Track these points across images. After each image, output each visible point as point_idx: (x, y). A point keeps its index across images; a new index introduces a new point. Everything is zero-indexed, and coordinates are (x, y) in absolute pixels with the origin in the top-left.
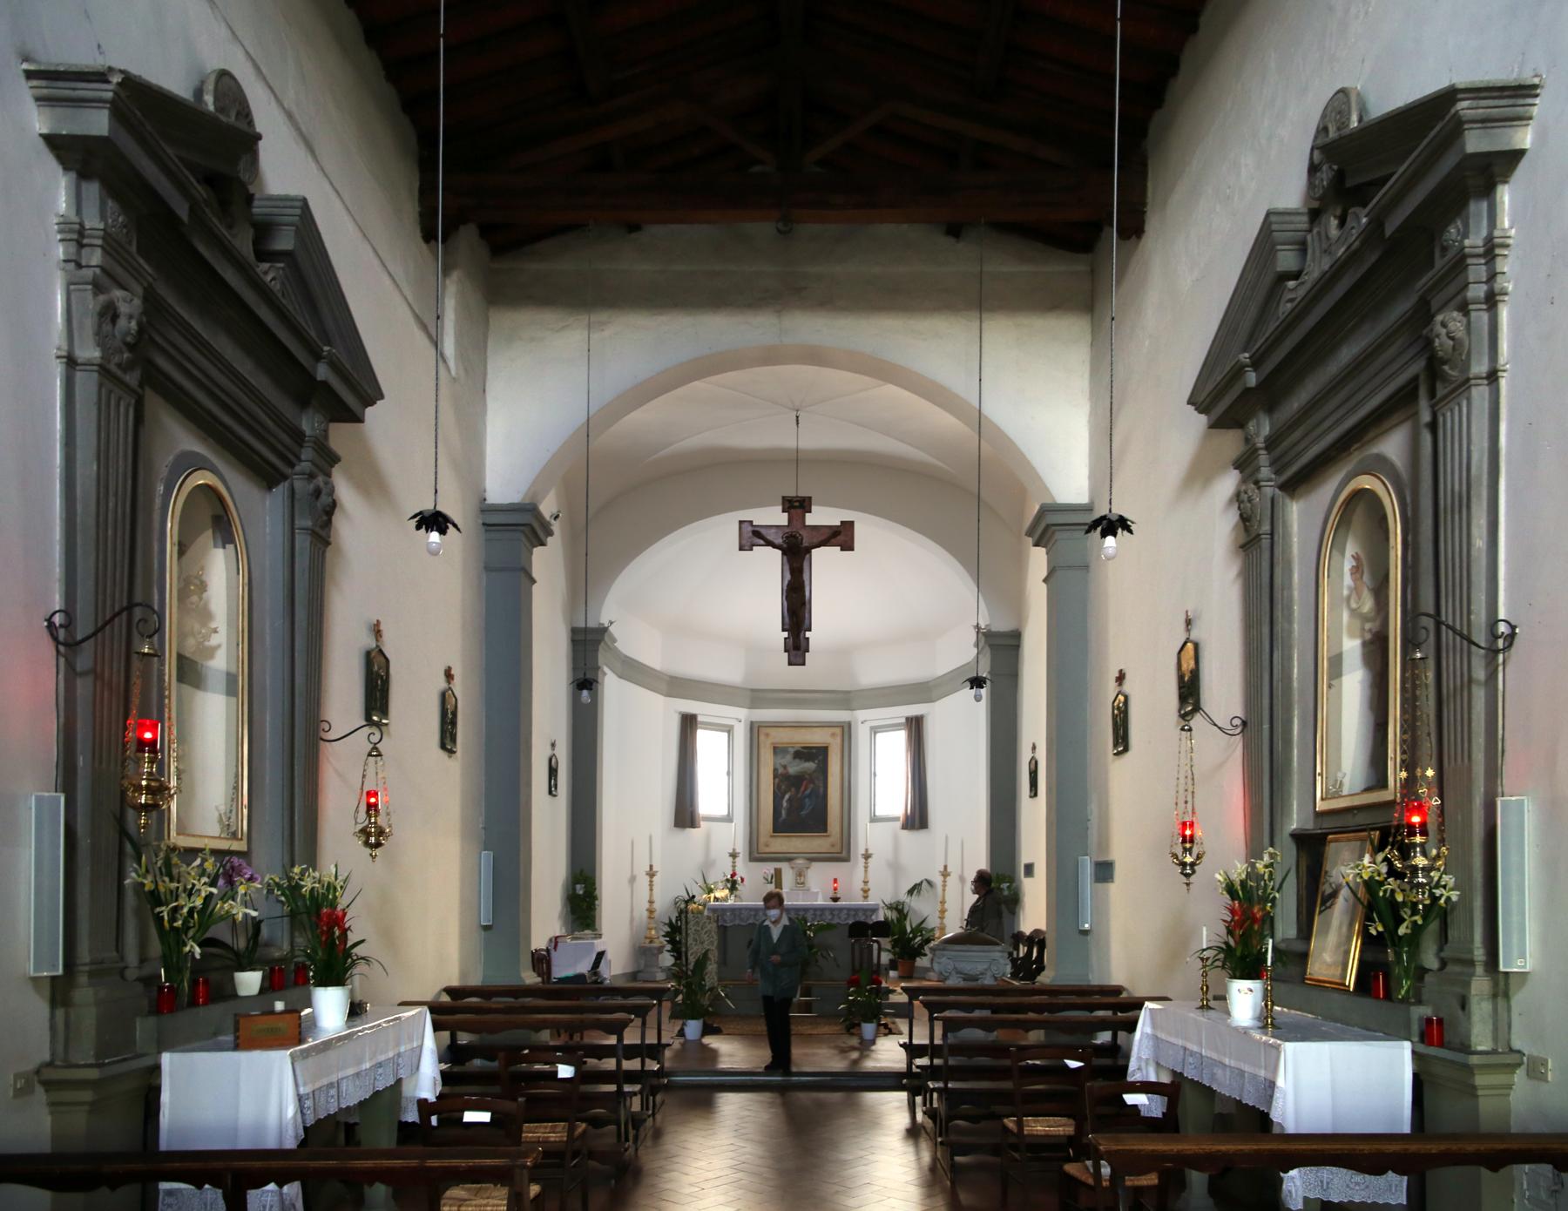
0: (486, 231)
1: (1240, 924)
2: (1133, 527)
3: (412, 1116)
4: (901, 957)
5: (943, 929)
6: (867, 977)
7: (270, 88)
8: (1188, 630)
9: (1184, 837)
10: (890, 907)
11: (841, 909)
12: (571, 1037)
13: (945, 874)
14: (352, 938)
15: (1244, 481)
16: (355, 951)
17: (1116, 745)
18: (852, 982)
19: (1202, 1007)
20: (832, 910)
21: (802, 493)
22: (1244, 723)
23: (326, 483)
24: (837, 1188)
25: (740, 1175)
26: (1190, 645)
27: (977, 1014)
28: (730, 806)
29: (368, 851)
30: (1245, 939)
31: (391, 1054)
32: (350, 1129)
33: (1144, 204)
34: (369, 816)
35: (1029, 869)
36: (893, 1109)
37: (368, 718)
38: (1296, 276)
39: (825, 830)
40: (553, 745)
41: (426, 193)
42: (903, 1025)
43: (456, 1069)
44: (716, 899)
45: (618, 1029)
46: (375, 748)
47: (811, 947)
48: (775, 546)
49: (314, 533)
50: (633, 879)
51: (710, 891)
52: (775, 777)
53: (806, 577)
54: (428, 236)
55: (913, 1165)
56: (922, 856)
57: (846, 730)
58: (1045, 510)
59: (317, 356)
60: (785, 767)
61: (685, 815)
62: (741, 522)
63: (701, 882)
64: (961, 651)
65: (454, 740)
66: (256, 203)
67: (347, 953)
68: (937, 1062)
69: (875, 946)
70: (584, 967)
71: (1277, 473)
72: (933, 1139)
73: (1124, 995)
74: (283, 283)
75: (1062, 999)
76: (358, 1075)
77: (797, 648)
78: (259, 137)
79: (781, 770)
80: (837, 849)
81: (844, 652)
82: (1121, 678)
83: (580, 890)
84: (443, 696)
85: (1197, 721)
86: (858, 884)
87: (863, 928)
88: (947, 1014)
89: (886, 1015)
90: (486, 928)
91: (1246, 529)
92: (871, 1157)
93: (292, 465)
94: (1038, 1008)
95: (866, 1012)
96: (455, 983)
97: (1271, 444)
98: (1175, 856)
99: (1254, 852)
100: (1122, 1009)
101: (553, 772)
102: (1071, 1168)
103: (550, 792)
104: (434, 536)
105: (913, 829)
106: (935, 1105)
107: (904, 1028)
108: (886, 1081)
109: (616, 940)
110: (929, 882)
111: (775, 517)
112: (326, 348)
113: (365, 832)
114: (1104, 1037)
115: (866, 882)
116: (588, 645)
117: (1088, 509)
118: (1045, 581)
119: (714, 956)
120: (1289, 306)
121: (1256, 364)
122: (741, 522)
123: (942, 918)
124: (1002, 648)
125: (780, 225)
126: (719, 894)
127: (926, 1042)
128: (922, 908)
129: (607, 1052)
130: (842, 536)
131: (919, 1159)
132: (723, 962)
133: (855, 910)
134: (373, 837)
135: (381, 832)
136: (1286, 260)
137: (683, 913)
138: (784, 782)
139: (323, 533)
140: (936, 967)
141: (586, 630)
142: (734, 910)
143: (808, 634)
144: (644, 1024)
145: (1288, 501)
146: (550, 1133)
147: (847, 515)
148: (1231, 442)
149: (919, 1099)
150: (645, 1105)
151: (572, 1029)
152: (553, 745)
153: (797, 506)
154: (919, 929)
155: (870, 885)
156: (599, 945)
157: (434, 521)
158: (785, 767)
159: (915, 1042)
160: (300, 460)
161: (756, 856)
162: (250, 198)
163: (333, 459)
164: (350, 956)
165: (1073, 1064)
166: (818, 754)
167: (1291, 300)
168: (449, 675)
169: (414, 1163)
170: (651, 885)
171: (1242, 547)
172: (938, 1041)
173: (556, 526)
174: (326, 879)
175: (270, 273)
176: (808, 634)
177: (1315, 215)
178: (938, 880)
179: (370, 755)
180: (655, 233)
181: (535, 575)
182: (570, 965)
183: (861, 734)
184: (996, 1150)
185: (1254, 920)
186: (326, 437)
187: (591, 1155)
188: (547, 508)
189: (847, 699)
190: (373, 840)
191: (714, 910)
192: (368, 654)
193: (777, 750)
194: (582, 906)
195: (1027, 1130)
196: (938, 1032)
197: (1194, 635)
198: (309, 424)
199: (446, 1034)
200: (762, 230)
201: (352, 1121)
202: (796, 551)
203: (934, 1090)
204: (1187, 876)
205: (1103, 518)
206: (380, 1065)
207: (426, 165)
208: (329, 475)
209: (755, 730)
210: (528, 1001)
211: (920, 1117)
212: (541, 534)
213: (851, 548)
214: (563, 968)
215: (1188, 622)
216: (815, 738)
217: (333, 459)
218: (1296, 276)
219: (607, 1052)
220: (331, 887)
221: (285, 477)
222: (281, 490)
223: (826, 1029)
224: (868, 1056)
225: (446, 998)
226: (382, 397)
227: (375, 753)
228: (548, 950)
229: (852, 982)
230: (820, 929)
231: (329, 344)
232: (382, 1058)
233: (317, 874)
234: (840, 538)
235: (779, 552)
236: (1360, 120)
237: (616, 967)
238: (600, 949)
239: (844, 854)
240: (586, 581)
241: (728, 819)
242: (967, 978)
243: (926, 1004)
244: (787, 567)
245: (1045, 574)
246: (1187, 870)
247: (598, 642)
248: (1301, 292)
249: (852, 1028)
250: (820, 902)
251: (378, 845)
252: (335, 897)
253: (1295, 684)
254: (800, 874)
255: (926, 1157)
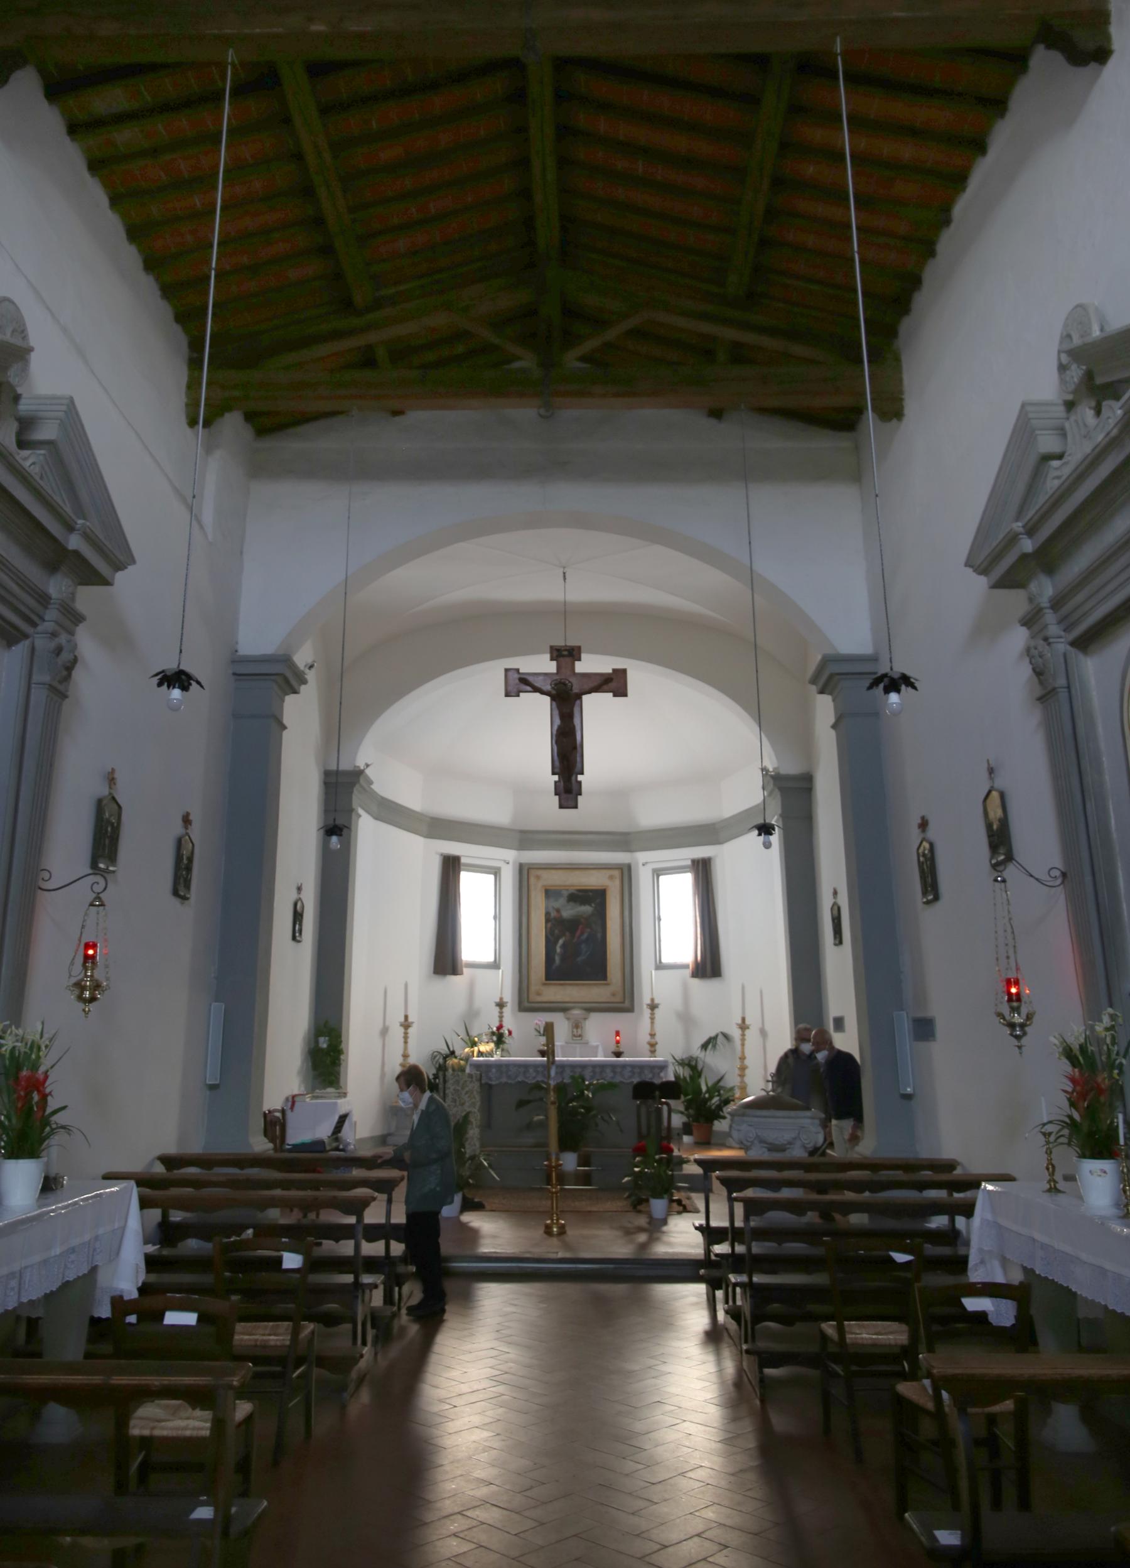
0: (249, 417)
1: (1083, 1096)
2: (917, 684)
3: (104, 1311)
4: (696, 1120)
5: (743, 1088)
6: (656, 1143)
7: (48, 308)
8: (991, 779)
9: (1009, 994)
10: (682, 1063)
11: (624, 1066)
12: (305, 1216)
13: (743, 1026)
14: (52, 1104)
15: (1033, 637)
16: (54, 1118)
17: (925, 893)
18: (639, 1150)
19: (1049, 1190)
20: (613, 1067)
21: (572, 642)
22: (1064, 875)
23: (69, 641)
24: (652, 1362)
25: (501, 1389)
26: (995, 794)
27: (786, 1193)
28: (498, 953)
29: (81, 1005)
30: (1091, 1113)
31: (87, 1237)
32: (33, 1324)
33: (901, 392)
34: (85, 968)
35: (839, 1023)
36: (690, 1306)
37: (94, 865)
38: (1060, 457)
39: (605, 978)
40: (299, 889)
41: (193, 385)
42: (698, 1200)
43: (165, 1252)
44: (480, 1054)
45: (358, 1207)
46: (98, 898)
47: (588, 1109)
48: (542, 692)
49: (52, 688)
50: (384, 1031)
51: (474, 1044)
52: (547, 921)
53: (576, 721)
54: (192, 422)
55: (714, 1378)
56: (716, 1008)
57: (626, 873)
58: (826, 661)
59: (70, 528)
60: (558, 911)
61: (446, 959)
62: (507, 670)
63: (463, 1034)
64: (746, 792)
65: (188, 886)
66: (22, 401)
67: (45, 1122)
68: (740, 1249)
69: (665, 1108)
70: (323, 1132)
71: (1066, 630)
72: (736, 1345)
73: (958, 1171)
74: (42, 467)
75: (885, 1175)
76: (45, 1262)
77: (568, 788)
78: (31, 349)
79: (553, 914)
80: (618, 999)
81: (621, 794)
82: (924, 825)
83: (323, 1043)
84: (179, 843)
85: (1010, 871)
86: (644, 1037)
87: (650, 1089)
88: (750, 1193)
89: (679, 1189)
90: (213, 1087)
91: (1041, 683)
92: (664, 1368)
93: (34, 625)
94: (858, 1186)
95: (655, 1185)
96: (172, 1149)
97: (1057, 604)
98: (1001, 1015)
99: (1092, 1013)
100: (958, 1186)
101: (298, 916)
102: (905, 1388)
103: (294, 938)
104: (176, 693)
105: (715, 968)
106: (739, 1303)
107: (701, 1206)
108: (681, 1270)
109: (364, 1100)
110: (726, 1036)
111: (543, 665)
112: (80, 522)
113: (79, 986)
114: (938, 1222)
115: (652, 1035)
116: (342, 792)
117: (874, 659)
118: (834, 727)
119: (476, 1119)
120: (1057, 483)
121: (1030, 532)
122: (507, 670)
123: (742, 1076)
124: (793, 792)
125: (542, 411)
126: (484, 1048)
127: (726, 1224)
128: (718, 1064)
129: (345, 1232)
130: (614, 684)
131: (720, 1371)
132: (487, 1125)
133: (641, 1067)
134: (88, 992)
135: (97, 986)
136: (1048, 443)
137: (442, 1068)
138: (557, 926)
139: (61, 687)
140: (735, 1134)
141: (337, 773)
142: (499, 1066)
143: (580, 777)
144: (390, 1201)
145: (1081, 656)
146: (272, 1335)
147: (619, 663)
148: (1016, 601)
149: (719, 1294)
150: (388, 1299)
151: (307, 1206)
152: (299, 889)
153: (566, 655)
154: (716, 1088)
155: (658, 1038)
156: (343, 1106)
157: (178, 679)
158: (558, 911)
159: (714, 1223)
160: (44, 620)
161: (526, 1004)
162: (17, 398)
163: (77, 618)
164: (48, 1123)
165: (900, 1257)
166: (596, 898)
167: (1058, 477)
168: (187, 820)
169: (97, 1379)
170: (406, 1037)
171: (1041, 699)
172: (739, 1223)
173: (311, 676)
174: (30, 1038)
175: (29, 460)
176: (580, 777)
177: (1070, 406)
178: (736, 1033)
179: (92, 905)
180: (417, 417)
181: (285, 721)
182: (305, 1130)
183: (643, 877)
184: (813, 1361)
185: (1100, 1091)
186: (73, 599)
187: (321, 1361)
188: (301, 659)
189: (626, 840)
190: (87, 994)
191: (478, 1066)
192: (100, 802)
193: (549, 893)
194: (325, 1060)
195: (849, 1337)
196: (739, 1209)
197: (999, 783)
198: (57, 587)
199: (156, 1214)
200: (525, 413)
201: (34, 1316)
202: (566, 699)
203: (735, 1285)
204: (1018, 1038)
205: (885, 676)
206: (73, 1250)
207: (195, 364)
208: (72, 633)
209: (524, 873)
210: (254, 1172)
211: (721, 1316)
212: (294, 683)
213: (625, 695)
214: (299, 1133)
215: (991, 771)
216: (592, 881)
217: (77, 618)
218: (1060, 457)
219: (345, 1232)
220: (35, 1047)
221: (26, 636)
222: (20, 649)
223: (610, 1206)
224: (658, 1239)
225: (159, 1169)
226: (133, 562)
227: (98, 902)
228: (283, 1111)
229: (639, 1150)
230: (600, 1089)
231: (85, 518)
232: (75, 1242)
233: (20, 1032)
234: (612, 685)
235: (547, 699)
236: (1102, 330)
237: (363, 1128)
238: (342, 1112)
239: (627, 1004)
240: (339, 727)
241: (495, 965)
242: (773, 1148)
243: (724, 1181)
244: (556, 712)
245: (832, 720)
246: (1018, 1031)
247: (353, 785)
248: (1066, 471)
249: (638, 1204)
250: (600, 1058)
251: (93, 999)
252: (38, 1057)
253: (1115, 835)
254: (577, 1025)
255: (730, 1367)
